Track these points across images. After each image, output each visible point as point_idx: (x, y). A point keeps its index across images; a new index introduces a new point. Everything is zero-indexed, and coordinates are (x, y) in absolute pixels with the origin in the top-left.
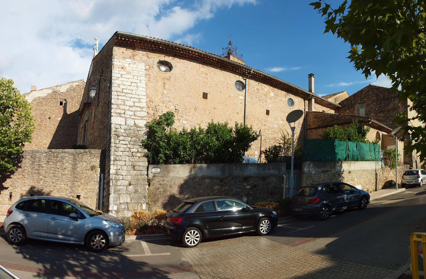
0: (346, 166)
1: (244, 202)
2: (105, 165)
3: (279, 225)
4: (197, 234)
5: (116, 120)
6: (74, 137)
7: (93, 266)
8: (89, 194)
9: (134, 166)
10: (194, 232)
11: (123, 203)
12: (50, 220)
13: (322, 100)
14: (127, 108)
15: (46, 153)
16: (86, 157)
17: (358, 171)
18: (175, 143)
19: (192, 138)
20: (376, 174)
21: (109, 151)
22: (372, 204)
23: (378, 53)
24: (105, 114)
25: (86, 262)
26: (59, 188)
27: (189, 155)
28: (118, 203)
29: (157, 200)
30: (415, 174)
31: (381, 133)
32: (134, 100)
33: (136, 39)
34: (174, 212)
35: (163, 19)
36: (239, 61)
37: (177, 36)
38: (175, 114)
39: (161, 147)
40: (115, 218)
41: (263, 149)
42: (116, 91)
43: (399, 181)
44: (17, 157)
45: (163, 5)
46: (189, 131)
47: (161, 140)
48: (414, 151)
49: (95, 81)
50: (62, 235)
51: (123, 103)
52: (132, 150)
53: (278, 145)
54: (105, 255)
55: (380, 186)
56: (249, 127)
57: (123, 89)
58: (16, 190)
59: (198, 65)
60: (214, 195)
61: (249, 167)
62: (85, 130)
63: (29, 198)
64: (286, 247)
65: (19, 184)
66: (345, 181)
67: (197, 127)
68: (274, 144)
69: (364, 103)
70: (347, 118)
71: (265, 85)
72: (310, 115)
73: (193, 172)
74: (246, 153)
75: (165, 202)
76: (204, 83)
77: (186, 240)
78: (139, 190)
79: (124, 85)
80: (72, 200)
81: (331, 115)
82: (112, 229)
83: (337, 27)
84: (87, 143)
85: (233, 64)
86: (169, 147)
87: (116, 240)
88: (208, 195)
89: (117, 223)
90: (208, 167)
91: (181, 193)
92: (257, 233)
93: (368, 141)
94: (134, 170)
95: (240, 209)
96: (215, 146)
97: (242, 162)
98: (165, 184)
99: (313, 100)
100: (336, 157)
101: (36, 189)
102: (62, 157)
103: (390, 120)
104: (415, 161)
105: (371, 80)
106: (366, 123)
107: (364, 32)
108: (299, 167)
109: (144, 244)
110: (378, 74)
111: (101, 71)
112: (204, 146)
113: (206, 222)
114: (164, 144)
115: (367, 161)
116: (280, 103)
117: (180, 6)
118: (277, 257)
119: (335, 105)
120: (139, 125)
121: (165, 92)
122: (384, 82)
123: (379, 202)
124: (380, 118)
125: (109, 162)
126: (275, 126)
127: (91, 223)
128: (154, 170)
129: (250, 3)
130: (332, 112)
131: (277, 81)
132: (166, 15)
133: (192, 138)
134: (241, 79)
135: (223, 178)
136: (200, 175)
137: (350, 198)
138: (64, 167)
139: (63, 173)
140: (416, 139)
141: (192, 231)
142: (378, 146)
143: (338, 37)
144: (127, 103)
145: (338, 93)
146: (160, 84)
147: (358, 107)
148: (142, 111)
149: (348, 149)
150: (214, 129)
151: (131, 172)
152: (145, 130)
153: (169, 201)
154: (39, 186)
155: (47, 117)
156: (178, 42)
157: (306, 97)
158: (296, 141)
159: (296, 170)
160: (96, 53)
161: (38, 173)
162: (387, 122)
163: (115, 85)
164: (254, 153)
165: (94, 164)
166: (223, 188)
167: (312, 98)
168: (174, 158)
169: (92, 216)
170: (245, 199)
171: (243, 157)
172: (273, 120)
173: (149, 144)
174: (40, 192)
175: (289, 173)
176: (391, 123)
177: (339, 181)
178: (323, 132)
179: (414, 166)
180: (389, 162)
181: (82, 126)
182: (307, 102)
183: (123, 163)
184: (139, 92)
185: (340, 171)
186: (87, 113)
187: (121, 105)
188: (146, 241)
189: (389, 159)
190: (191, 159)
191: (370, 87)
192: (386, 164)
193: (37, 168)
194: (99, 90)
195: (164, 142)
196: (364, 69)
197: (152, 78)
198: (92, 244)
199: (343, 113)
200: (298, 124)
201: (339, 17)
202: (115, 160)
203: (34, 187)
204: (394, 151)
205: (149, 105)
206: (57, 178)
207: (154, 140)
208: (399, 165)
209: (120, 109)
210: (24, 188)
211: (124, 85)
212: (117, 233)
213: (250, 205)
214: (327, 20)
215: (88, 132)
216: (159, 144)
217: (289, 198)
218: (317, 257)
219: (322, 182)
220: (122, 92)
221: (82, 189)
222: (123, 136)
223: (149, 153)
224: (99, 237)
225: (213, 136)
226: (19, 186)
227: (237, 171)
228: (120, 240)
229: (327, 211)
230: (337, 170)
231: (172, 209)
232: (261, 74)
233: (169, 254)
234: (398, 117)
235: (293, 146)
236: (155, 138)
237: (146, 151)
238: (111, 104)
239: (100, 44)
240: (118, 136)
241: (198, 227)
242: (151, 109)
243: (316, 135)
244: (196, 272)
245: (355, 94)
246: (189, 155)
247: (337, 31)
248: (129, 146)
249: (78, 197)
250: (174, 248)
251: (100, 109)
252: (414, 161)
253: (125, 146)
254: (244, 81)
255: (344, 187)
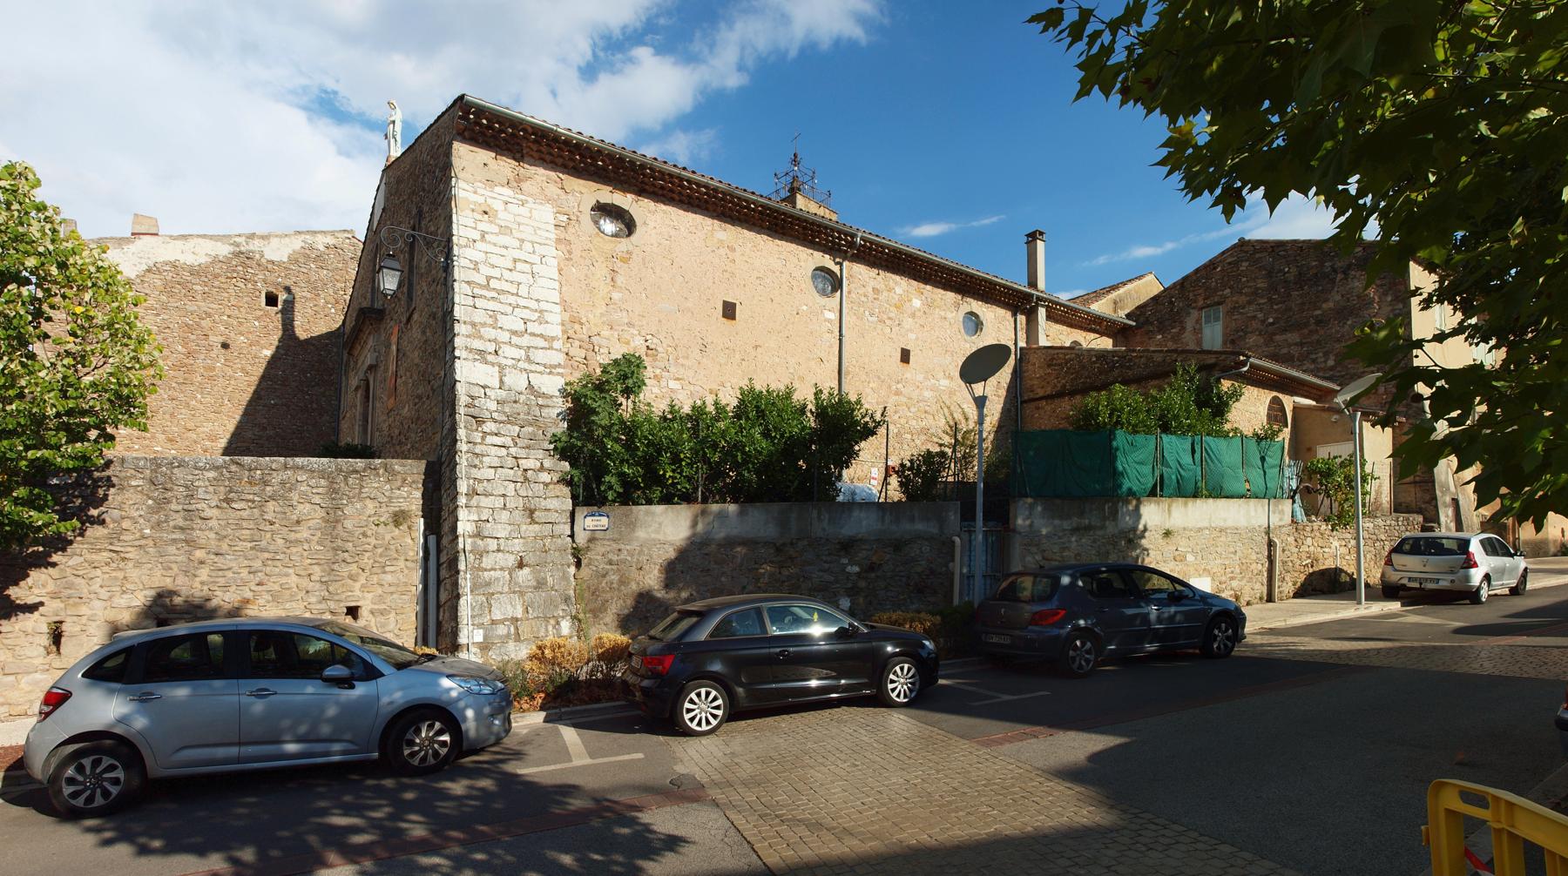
0: (1152, 514)
1: (843, 611)
2: (440, 510)
3: (941, 682)
4: (715, 699)
5: (468, 373)
6: (326, 418)
7: (414, 817)
8: (389, 598)
9: (532, 512)
10: (708, 694)
11: (502, 622)
12: (245, 699)
13: (1072, 309)
14: (505, 336)
15: (216, 468)
16: (376, 484)
17: (1200, 530)
18: (647, 446)
19: (695, 429)
20: (1271, 544)
21: (453, 465)
22: (1254, 646)
23: (1274, 126)
24: (434, 351)
25: (387, 810)
26: (277, 587)
27: (689, 479)
28: (486, 620)
29: (603, 608)
30: (1450, 552)
31: (1289, 402)
32: (526, 314)
33: (524, 130)
34: (652, 638)
35: (604, 79)
36: (821, 212)
37: (648, 136)
38: (647, 361)
39: (609, 456)
40: (480, 667)
41: (894, 462)
42: (468, 283)
43: (1372, 573)
44: (78, 484)
45: (602, 37)
46: (687, 410)
47: (608, 435)
48: (1442, 463)
49: (395, 241)
50: (298, 741)
51: (490, 321)
52: (524, 464)
53: (935, 449)
54: (452, 780)
55: (1286, 586)
56: (853, 398)
57: (489, 278)
58: (84, 610)
59: (709, 221)
60: (759, 590)
61: (856, 513)
62: (367, 397)
63: (153, 632)
64: (964, 745)
65: (96, 587)
66: (1151, 561)
67: (710, 400)
68: (924, 448)
69: (1219, 303)
70: (1158, 358)
71: (897, 278)
72: (1033, 358)
73: (700, 527)
74: (845, 472)
75: (626, 612)
76: (727, 275)
77: (687, 717)
78: (550, 580)
79: (493, 266)
80: (329, 623)
81: (1102, 355)
82: (471, 699)
83: (1118, 75)
84: (377, 441)
85: (806, 221)
86: (633, 456)
87: (483, 731)
88: (743, 590)
89: (485, 680)
90: (741, 513)
91: (668, 585)
92: (880, 700)
93: (1235, 430)
94: (533, 522)
95: (833, 629)
96: (760, 453)
97: (834, 498)
98: (624, 561)
99: (1042, 312)
100: (1120, 486)
101: (178, 600)
102: (283, 483)
103: (1326, 354)
104: (1448, 499)
105: (1248, 224)
106: (1230, 369)
107: (1219, 67)
108: (999, 513)
109: (569, 734)
110: (1273, 200)
111: (414, 212)
112: (728, 454)
113: (738, 664)
114: (618, 447)
115: (1232, 497)
116: (939, 327)
117: (652, 46)
118: (938, 772)
119: (1114, 322)
120: (544, 390)
121: (616, 296)
122: (1306, 218)
123: (1281, 639)
124: (1285, 351)
125: (455, 498)
126: (927, 394)
127: (402, 689)
128: (590, 522)
129: (850, 39)
130: (1106, 343)
131: (930, 263)
132: (613, 70)
133: (695, 429)
134: (827, 261)
135: (784, 544)
136: (720, 535)
137: (1171, 618)
138: (295, 518)
139: (292, 536)
140: (1454, 414)
141: (703, 691)
142: (1276, 449)
143: (1123, 103)
144: (503, 321)
145: (1124, 284)
146: (601, 271)
147: (1198, 321)
148: (551, 348)
149: (1160, 458)
150: (757, 407)
151: (524, 527)
152: (561, 405)
153: (635, 608)
154: (191, 587)
155: (216, 340)
156: (649, 152)
157: (1020, 303)
158: (991, 437)
159: (990, 524)
160: (396, 152)
161: (186, 541)
162: (1314, 361)
163: (463, 262)
164: (867, 474)
165: (404, 506)
166: (785, 572)
167: (1037, 305)
168: (648, 487)
169: (401, 666)
170: (845, 603)
171: (839, 485)
172: (920, 377)
173: (573, 446)
174: (200, 607)
175: (970, 532)
176: (1331, 363)
177: (1130, 561)
178: (1073, 407)
179: (1443, 519)
180: (1327, 502)
181: (354, 382)
182: (1022, 318)
183: (499, 502)
184: (536, 292)
185: (1135, 529)
186: (371, 343)
187: (484, 325)
188: (575, 726)
189: (1325, 491)
190: (696, 489)
191: (1245, 248)
192: (1311, 510)
193: (181, 522)
194: (411, 271)
195: (617, 440)
196: (1218, 191)
197: (577, 253)
198: (406, 752)
199: (1142, 343)
200: (996, 387)
201: (1123, 40)
202: (473, 493)
203: (172, 593)
204: (1350, 462)
205: (571, 333)
206: (266, 555)
207: (589, 437)
208: (1370, 515)
209: (481, 337)
210: (122, 601)
211: (493, 266)
212: (487, 710)
213: (860, 620)
214: (1083, 57)
215: (378, 405)
216: (603, 447)
217: (971, 603)
218: (1061, 788)
219: (1073, 562)
220: (487, 287)
221: (363, 586)
222: (495, 421)
223: (576, 472)
224: (431, 727)
225: (753, 426)
226: (93, 591)
227: (821, 525)
228: (495, 729)
229: (1088, 652)
230: (1122, 525)
231: (645, 632)
232: (883, 246)
233: (640, 756)
234: (1365, 340)
235: (980, 453)
236: (591, 430)
237: (566, 466)
238: (453, 320)
239: (407, 125)
240: (480, 421)
241: (717, 680)
242: (577, 343)
243: (1050, 417)
244: (715, 804)
245: (1185, 279)
246: (689, 479)
247: (1118, 85)
248: (513, 451)
249: (353, 612)
250: (655, 737)
251: (415, 333)
252: (1444, 499)
253: (503, 452)
254: (836, 269)
255: (1149, 579)
